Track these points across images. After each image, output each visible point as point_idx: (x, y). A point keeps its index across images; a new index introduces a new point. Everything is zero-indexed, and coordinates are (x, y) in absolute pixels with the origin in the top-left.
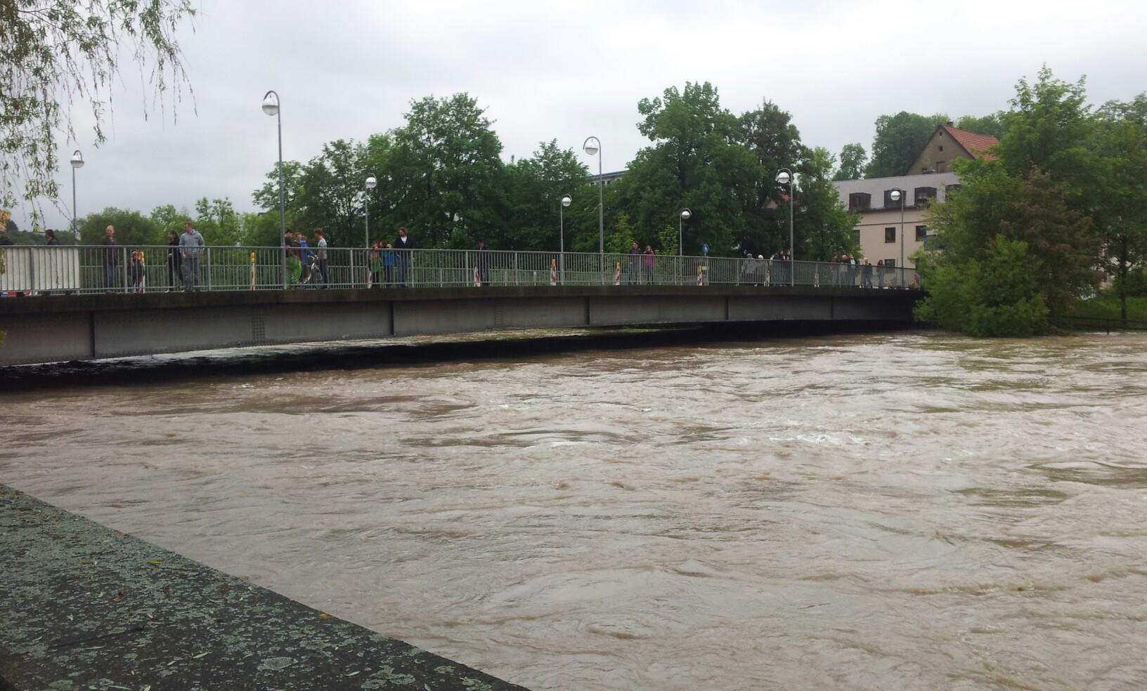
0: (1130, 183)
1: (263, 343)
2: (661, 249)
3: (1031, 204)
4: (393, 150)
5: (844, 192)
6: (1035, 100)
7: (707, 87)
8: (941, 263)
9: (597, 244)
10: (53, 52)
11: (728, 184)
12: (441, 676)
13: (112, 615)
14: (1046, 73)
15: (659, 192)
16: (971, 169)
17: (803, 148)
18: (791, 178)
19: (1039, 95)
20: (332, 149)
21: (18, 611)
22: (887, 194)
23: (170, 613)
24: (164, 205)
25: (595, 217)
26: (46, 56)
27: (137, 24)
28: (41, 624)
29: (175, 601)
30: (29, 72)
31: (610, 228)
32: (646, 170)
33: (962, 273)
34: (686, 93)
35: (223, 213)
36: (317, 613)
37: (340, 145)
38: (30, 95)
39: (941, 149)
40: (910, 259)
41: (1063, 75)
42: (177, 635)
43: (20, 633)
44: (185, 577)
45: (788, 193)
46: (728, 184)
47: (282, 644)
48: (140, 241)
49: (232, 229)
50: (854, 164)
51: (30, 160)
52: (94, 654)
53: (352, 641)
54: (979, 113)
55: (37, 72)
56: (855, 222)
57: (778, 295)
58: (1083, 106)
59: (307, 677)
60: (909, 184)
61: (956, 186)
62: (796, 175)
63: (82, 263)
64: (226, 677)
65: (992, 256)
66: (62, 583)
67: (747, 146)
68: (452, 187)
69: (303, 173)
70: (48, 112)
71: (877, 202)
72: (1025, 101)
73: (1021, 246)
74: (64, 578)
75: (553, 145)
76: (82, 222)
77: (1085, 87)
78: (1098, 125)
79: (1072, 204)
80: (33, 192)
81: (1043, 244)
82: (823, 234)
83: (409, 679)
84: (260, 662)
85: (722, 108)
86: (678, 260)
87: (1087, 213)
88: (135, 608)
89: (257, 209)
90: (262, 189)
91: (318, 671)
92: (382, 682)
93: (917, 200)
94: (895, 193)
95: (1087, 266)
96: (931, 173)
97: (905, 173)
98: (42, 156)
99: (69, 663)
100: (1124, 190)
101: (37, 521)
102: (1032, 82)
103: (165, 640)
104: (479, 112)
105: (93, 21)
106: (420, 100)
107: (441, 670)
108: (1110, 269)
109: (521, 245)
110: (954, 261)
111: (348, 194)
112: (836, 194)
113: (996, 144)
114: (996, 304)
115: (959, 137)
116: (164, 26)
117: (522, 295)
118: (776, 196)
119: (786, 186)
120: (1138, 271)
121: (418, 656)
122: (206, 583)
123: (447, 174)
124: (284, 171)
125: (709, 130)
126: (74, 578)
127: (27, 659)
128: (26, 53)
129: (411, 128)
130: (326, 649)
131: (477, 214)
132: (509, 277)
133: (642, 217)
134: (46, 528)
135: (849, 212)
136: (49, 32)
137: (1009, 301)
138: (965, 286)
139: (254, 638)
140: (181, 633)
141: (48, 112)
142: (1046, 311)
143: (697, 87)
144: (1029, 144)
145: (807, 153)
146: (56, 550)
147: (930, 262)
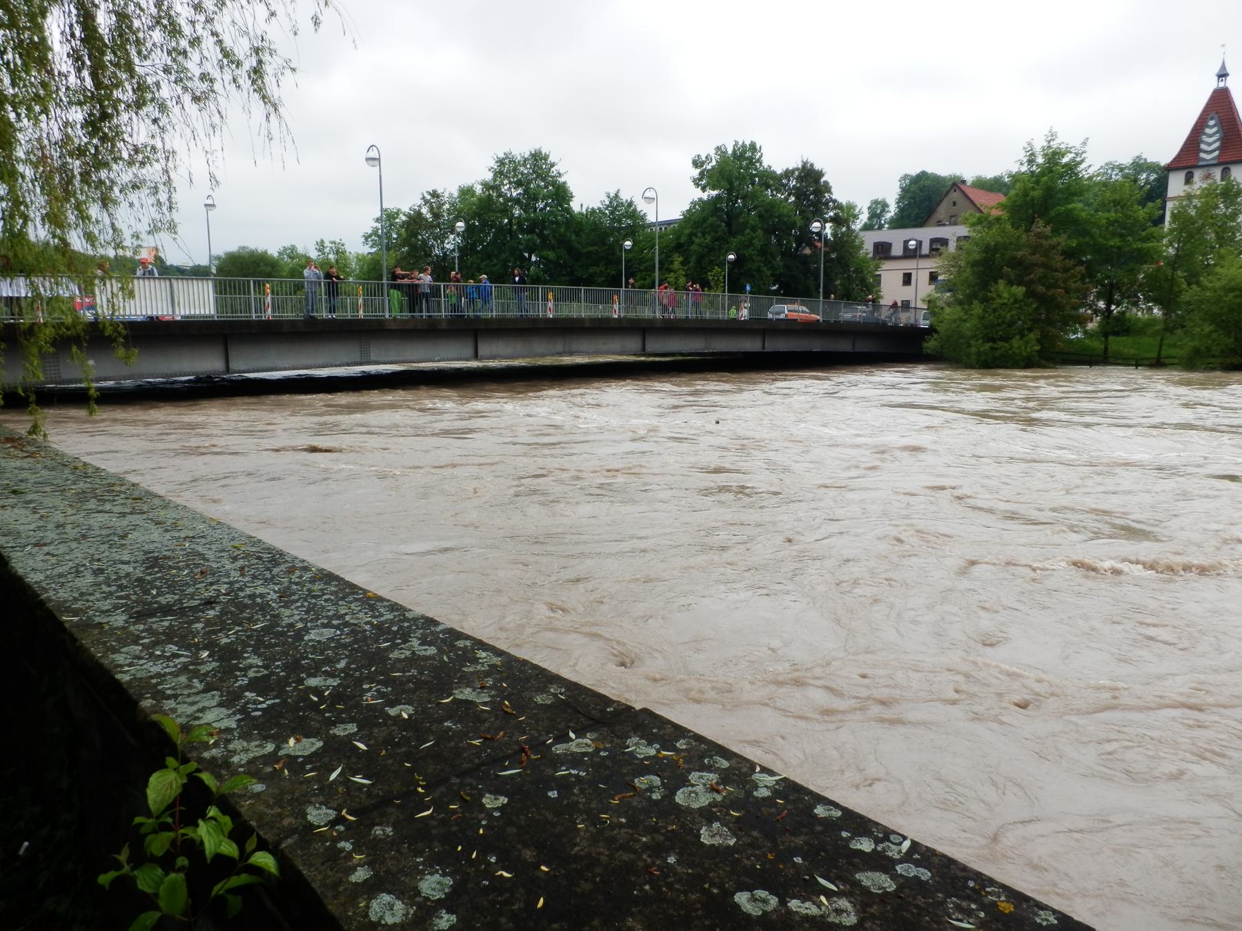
0: (1121, 236)
1: (369, 363)
2: (710, 288)
3: (1033, 254)
4: (480, 199)
5: (868, 241)
6: (1040, 160)
7: (753, 147)
8: (949, 305)
9: (654, 282)
10: (169, 103)
11: (769, 231)
12: (460, 649)
13: (191, 590)
14: (1052, 136)
15: (708, 238)
16: (979, 222)
17: (834, 201)
18: (823, 228)
19: (1045, 155)
20: (428, 197)
21: (109, 586)
22: (906, 242)
23: (241, 589)
24: (288, 245)
25: (653, 259)
26: (163, 107)
27: (245, 82)
28: (127, 597)
29: (247, 579)
30: (148, 122)
31: (665, 266)
32: (698, 219)
33: (966, 313)
34: (734, 151)
35: (338, 252)
36: (365, 591)
37: (434, 194)
38: (152, 142)
39: (955, 204)
40: (923, 301)
41: (1068, 138)
42: (242, 607)
43: (106, 605)
44: (259, 558)
45: (820, 240)
46: (769, 231)
47: (330, 618)
48: (270, 275)
49: (345, 266)
50: (879, 216)
51: (152, 200)
52: (166, 624)
53: (389, 616)
54: (989, 172)
55: (155, 121)
56: (877, 268)
57: (808, 329)
58: (1083, 166)
59: (345, 646)
60: (925, 234)
61: (966, 237)
62: (828, 225)
63: (216, 292)
64: (277, 645)
65: (994, 299)
66: (153, 562)
67: (786, 199)
68: (530, 231)
69: (404, 218)
70: (167, 159)
71: (897, 250)
72: (1031, 161)
73: (1019, 291)
74: (157, 558)
75: (617, 196)
76: (218, 258)
77: (1086, 149)
78: (1096, 184)
79: (1068, 254)
80: (154, 230)
81: (1040, 289)
82: (849, 278)
83: (432, 651)
84: (308, 633)
85: (765, 164)
86: (724, 296)
87: (1081, 263)
88: (211, 584)
89: (366, 250)
90: (370, 232)
91: (355, 642)
92: (408, 653)
93: (932, 249)
94: (913, 242)
95: (1076, 308)
96: (944, 225)
97: (922, 225)
98: (163, 197)
99: (142, 631)
100: (1115, 242)
101: (145, 509)
102: (1039, 144)
103: (231, 612)
104: (553, 165)
105: (204, 77)
106: (501, 156)
107: (460, 643)
108: (1096, 312)
109: (588, 282)
110: (960, 303)
111: (442, 238)
112: (862, 243)
113: (1002, 199)
114: (994, 340)
115: (972, 194)
116: (269, 80)
117: (587, 325)
118: (810, 243)
119: (819, 234)
120: (1123, 313)
121: (445, 631)
122: (277, 564)
123: (527, 220)
124: (389, 217)
125: (753, 184)
126: (165, 557)
127: (107, 627)
128: (144, 104)
129: (495, 180)
130: (366, 623)
131: (551, 255)
132: (581, 310)
133: (693, 259)
134: (151, 515)
135: (873, 259)
136: (164, 85)
137: (1006, 339)
138: (968, 325)
139: (307, 612)
140: (246, 606)
141: (167, 159)
142: (1037, 348)
143: (744, 145)
144: (1033, 199)
145: (839, 206)
146: (156, 534)
147: (939, 303)
